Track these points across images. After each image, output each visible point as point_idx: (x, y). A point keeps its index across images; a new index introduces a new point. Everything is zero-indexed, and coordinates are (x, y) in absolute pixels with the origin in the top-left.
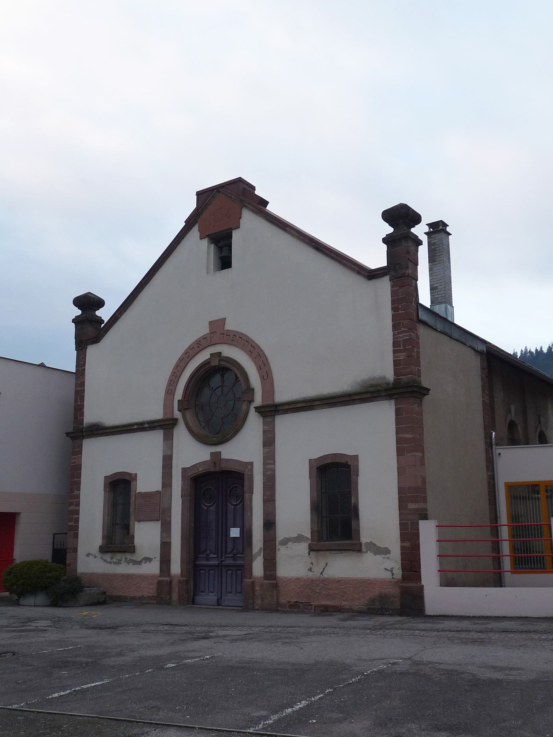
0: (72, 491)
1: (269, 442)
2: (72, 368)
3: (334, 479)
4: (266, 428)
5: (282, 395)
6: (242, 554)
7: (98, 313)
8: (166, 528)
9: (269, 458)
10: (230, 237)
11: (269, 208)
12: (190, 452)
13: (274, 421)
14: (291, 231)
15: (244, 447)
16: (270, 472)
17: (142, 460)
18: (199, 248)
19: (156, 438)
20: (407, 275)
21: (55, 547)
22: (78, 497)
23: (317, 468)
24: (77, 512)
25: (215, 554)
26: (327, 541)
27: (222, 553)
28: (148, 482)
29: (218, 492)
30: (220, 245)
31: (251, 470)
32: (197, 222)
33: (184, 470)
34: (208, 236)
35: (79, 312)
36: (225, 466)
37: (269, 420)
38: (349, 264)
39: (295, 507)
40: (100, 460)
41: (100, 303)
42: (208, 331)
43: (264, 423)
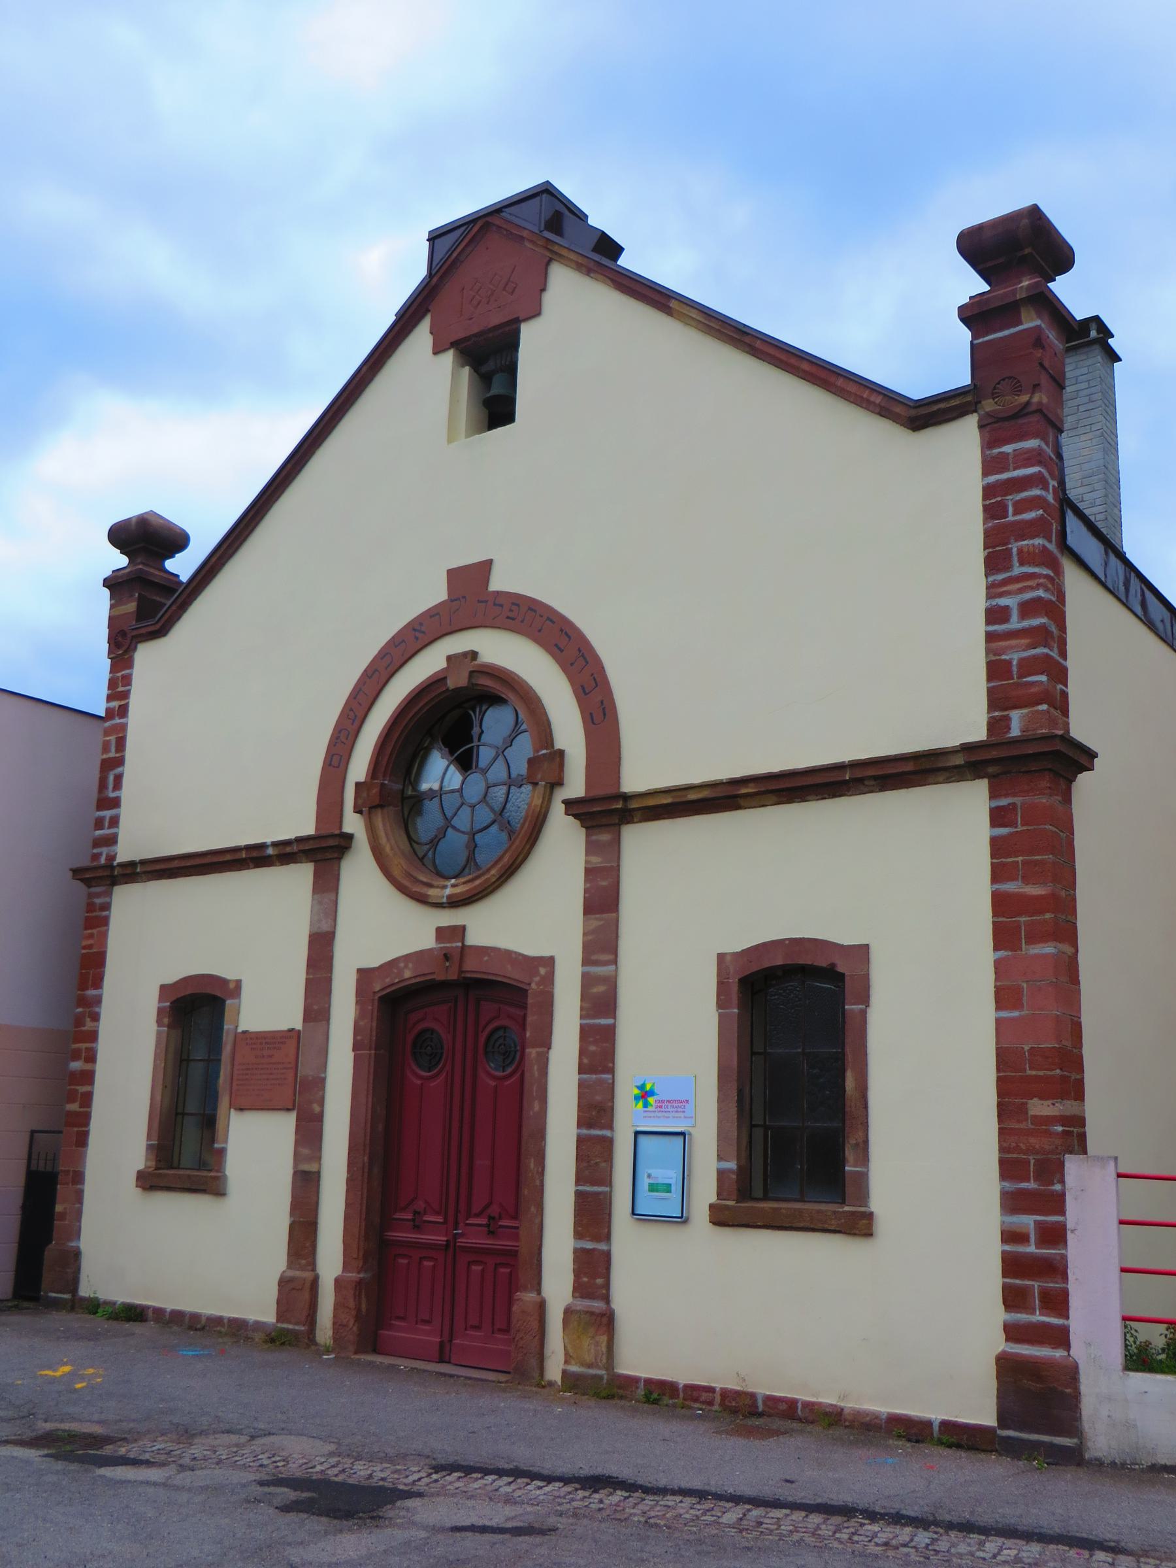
0: (79, 1021)
1: (602, 900)
2: (125, 852)
3: (795, 1026)
4: (596, 860)
5: (639, 775)
6: (515, 1217)
7: (171, 565)
8: (309, 1133)
9: (602, 945)
10: (515, 346)
11: (623, 261)
12: (383, 926)
13: (617, 841)
14: (685, 310)
15: (532, 917)
16: (601, 989)
17: (252, 944)
18: (430, 377)
19: (298, 879)
20: (1032, 408)
21: (33, 1168)
22: (93, 1036)
23: (741, 980)
24: (88, 1077)
25: (438, 1213)
26: (765, 1198)
27: (457, 1211)
28: (268, 1004)
29: (452, 1040)
30: (484, 369)
31: (549, 979)
32: (428, 311)
33: (364, 975)
34: (453, 345)
35: (122, 561)
36: (472, 966)
37: (605, 837)
38: (852, 388)
39: (675, 1053)
40: (154, 942)
41: (177, 541)
42: (443, 596)
43: (591, 848)
